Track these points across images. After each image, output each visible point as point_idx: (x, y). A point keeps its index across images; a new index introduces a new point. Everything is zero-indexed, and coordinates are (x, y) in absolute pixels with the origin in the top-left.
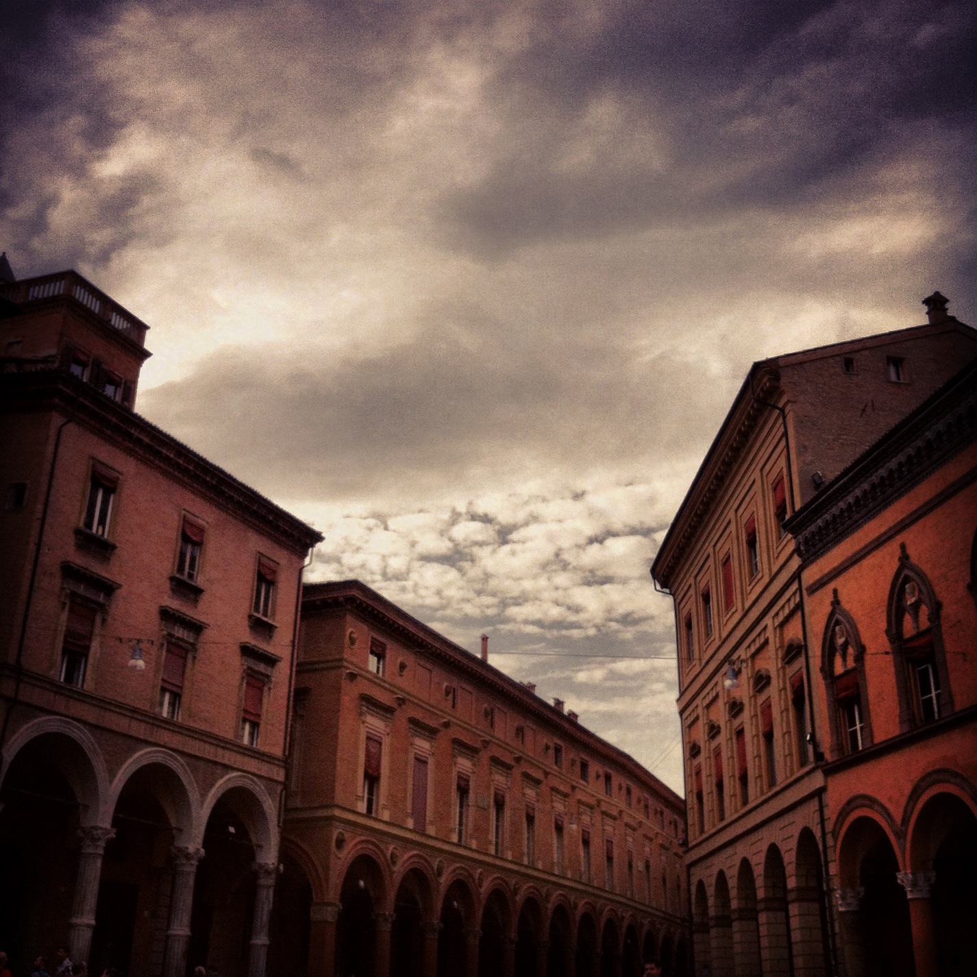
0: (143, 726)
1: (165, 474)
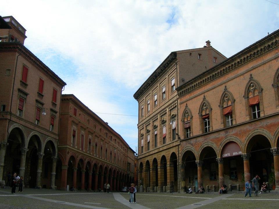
0: (33, 126)
1: (37, 68)
